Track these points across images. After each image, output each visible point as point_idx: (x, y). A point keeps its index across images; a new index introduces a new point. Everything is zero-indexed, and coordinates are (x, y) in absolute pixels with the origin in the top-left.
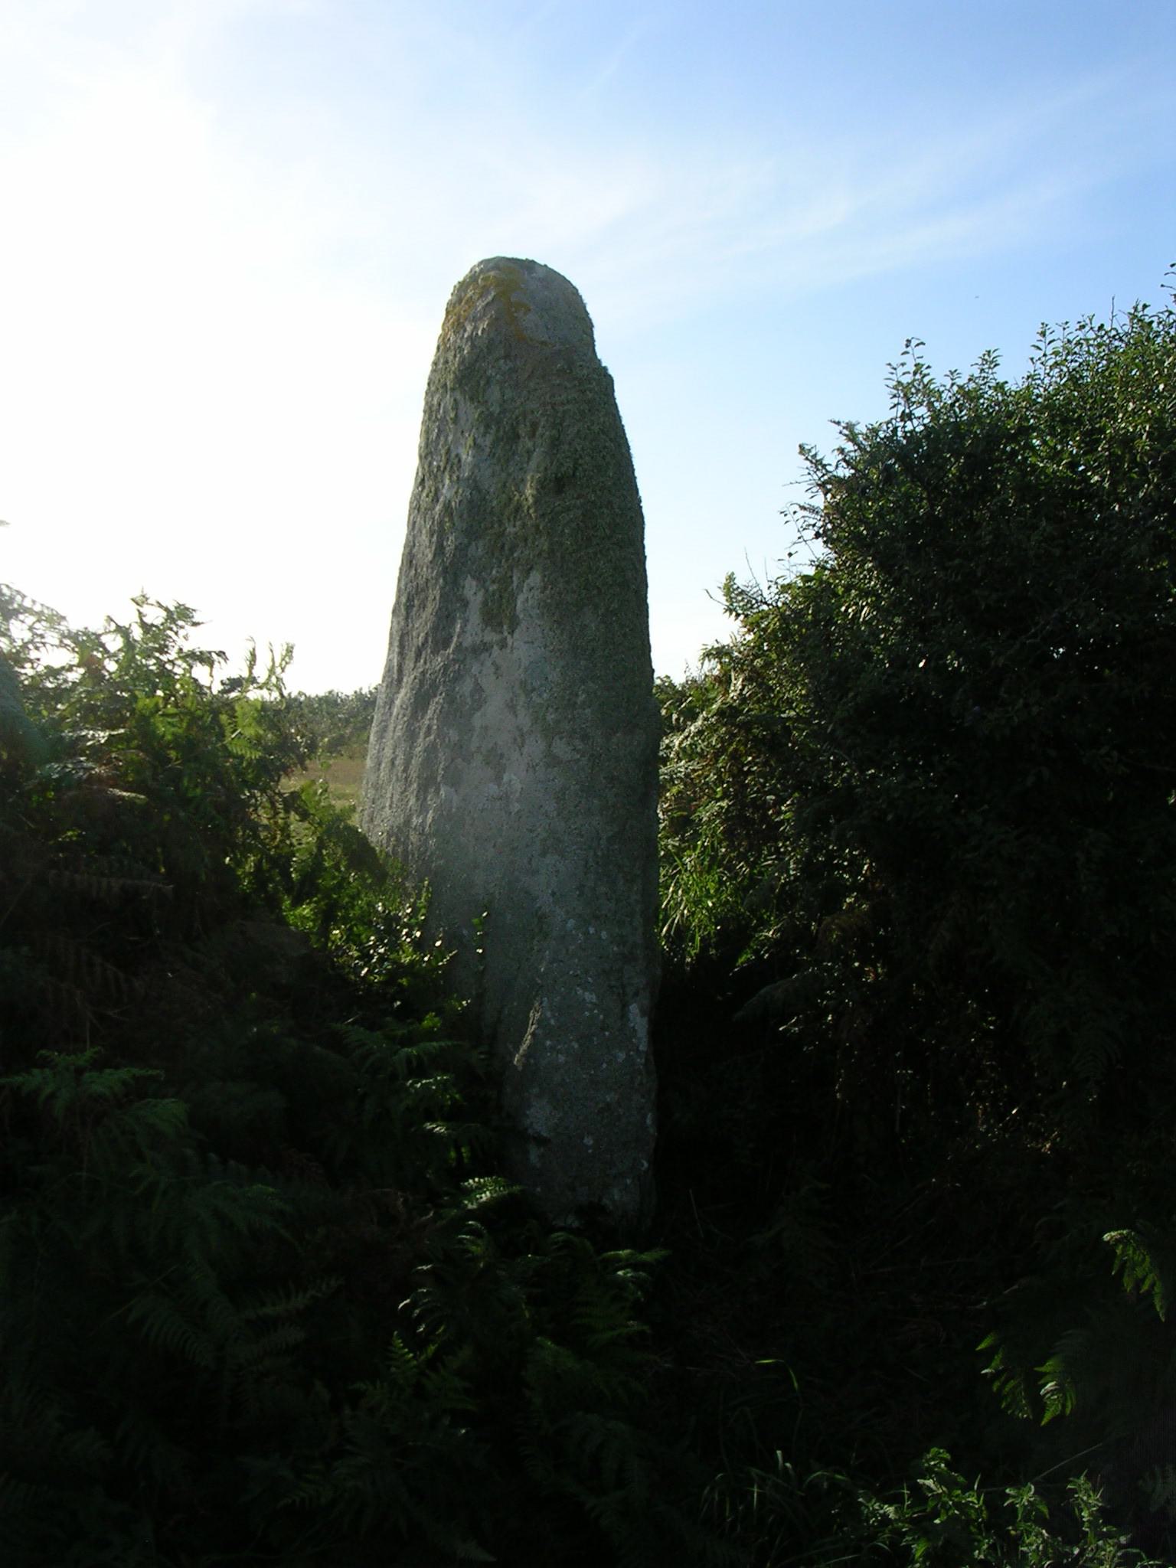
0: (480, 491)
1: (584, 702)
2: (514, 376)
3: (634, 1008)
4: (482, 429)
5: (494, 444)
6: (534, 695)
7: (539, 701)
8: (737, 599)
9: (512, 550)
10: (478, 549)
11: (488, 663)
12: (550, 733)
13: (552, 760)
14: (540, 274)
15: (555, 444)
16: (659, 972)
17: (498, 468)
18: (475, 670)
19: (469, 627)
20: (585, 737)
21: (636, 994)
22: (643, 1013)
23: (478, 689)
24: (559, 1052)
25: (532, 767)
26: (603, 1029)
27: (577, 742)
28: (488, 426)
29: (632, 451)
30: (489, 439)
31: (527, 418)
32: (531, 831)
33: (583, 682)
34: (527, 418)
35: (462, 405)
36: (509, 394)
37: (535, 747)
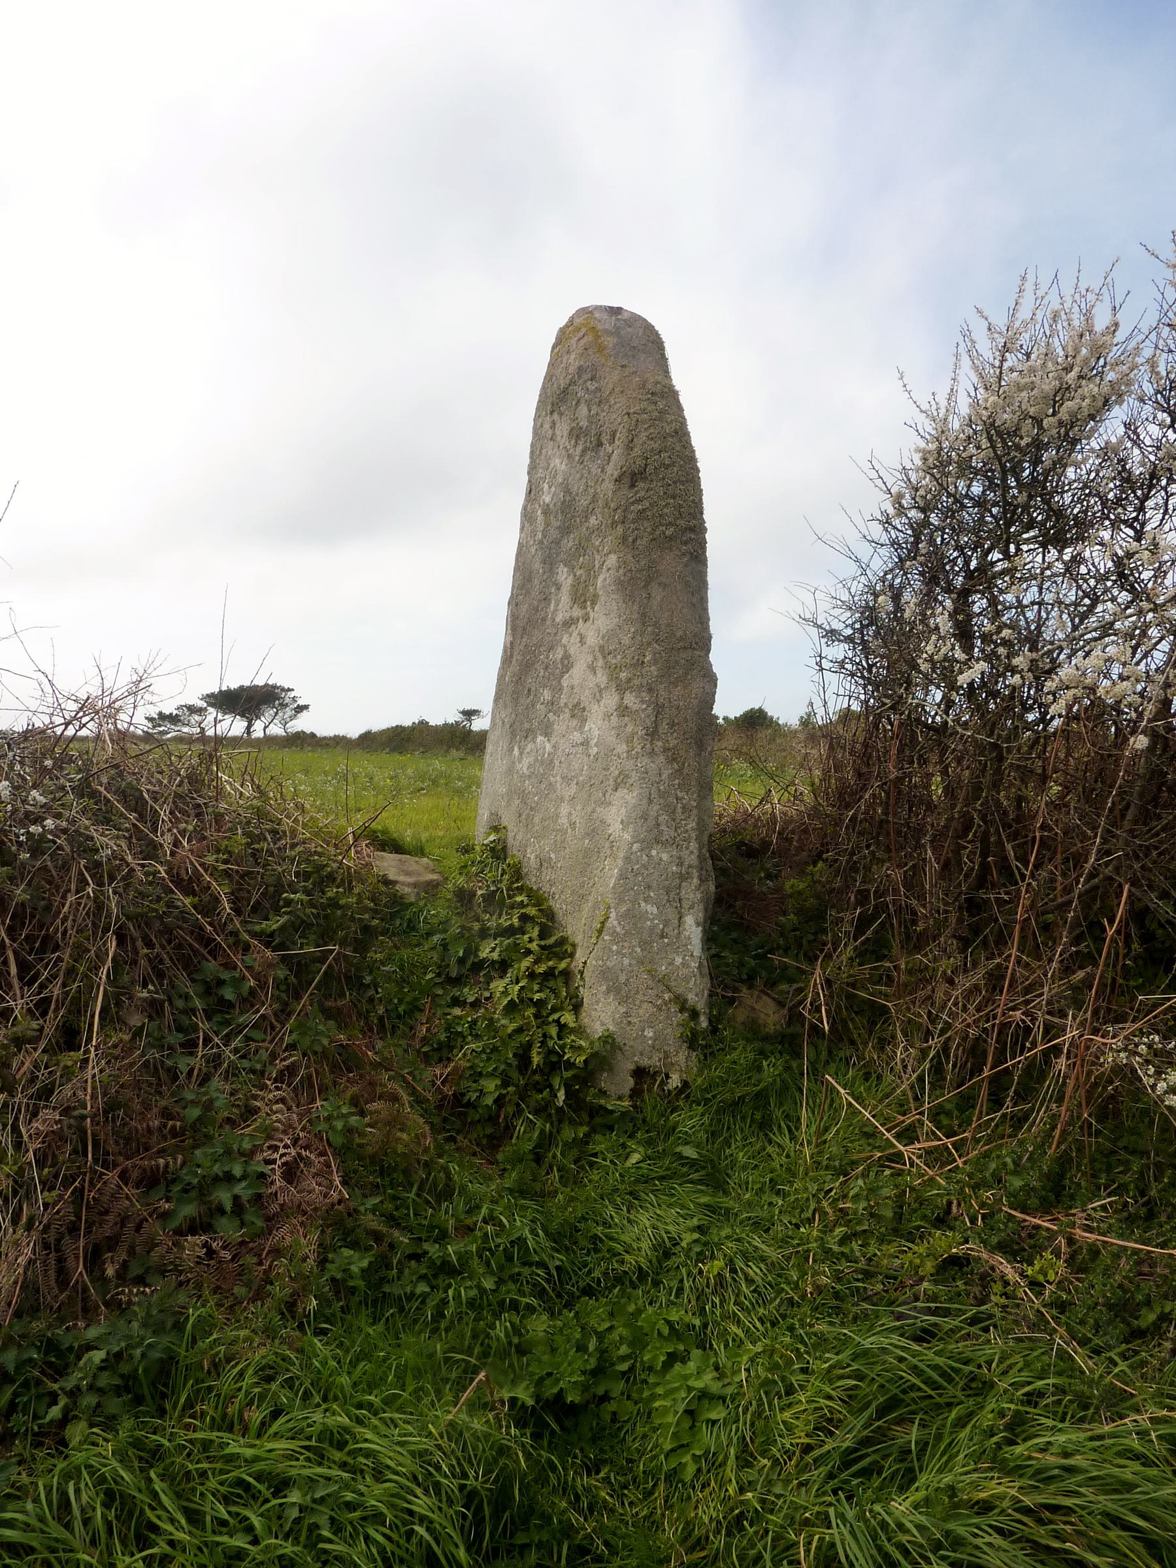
3: (689, 920)
6: (610, 658)
11: (575, 634)
12: (622, 688)
13: (623, 711)
14: (626, 316)
15: (629, 446)
16: (712, 888)
18: (564, 641)
21: (692, 907)
22: (698, 924)
23: (567, 656)
24: (624, 955)
25: (608, 716)
26: (662, 937)
28: (578, 437)
30: (579, 448)
31: (620, 461)
34: (620, 461)
37: (611, 700)
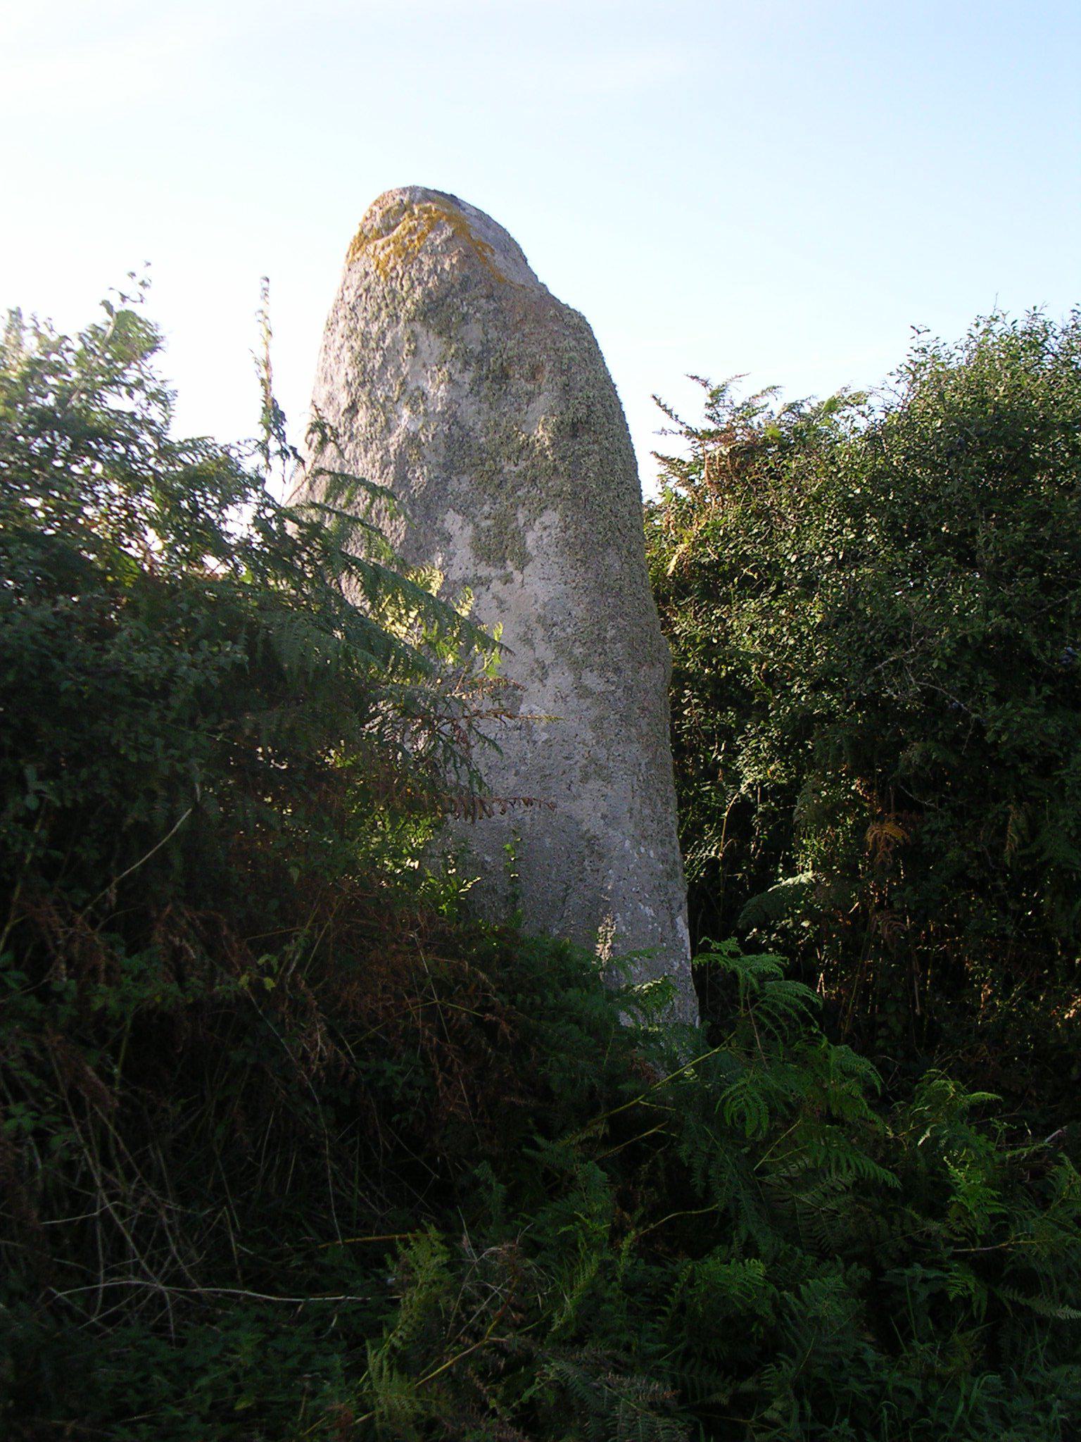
0: (462, 428)
1: (614, 638)
2: (501, 317)
4: (459, 366)
5: (478, 381)
6: (556, 630)
7: (563, 635)
8: (127, 339)
9: (515, 489)
10: (462, 485)
17: (485, 406)
19: (455, 561)
20: (617, 670)
27: (609, 674)
29: (621, 395)
32: (567, 758)
33: (612, 618)
35: (422, 338)
36: (493, 334)
